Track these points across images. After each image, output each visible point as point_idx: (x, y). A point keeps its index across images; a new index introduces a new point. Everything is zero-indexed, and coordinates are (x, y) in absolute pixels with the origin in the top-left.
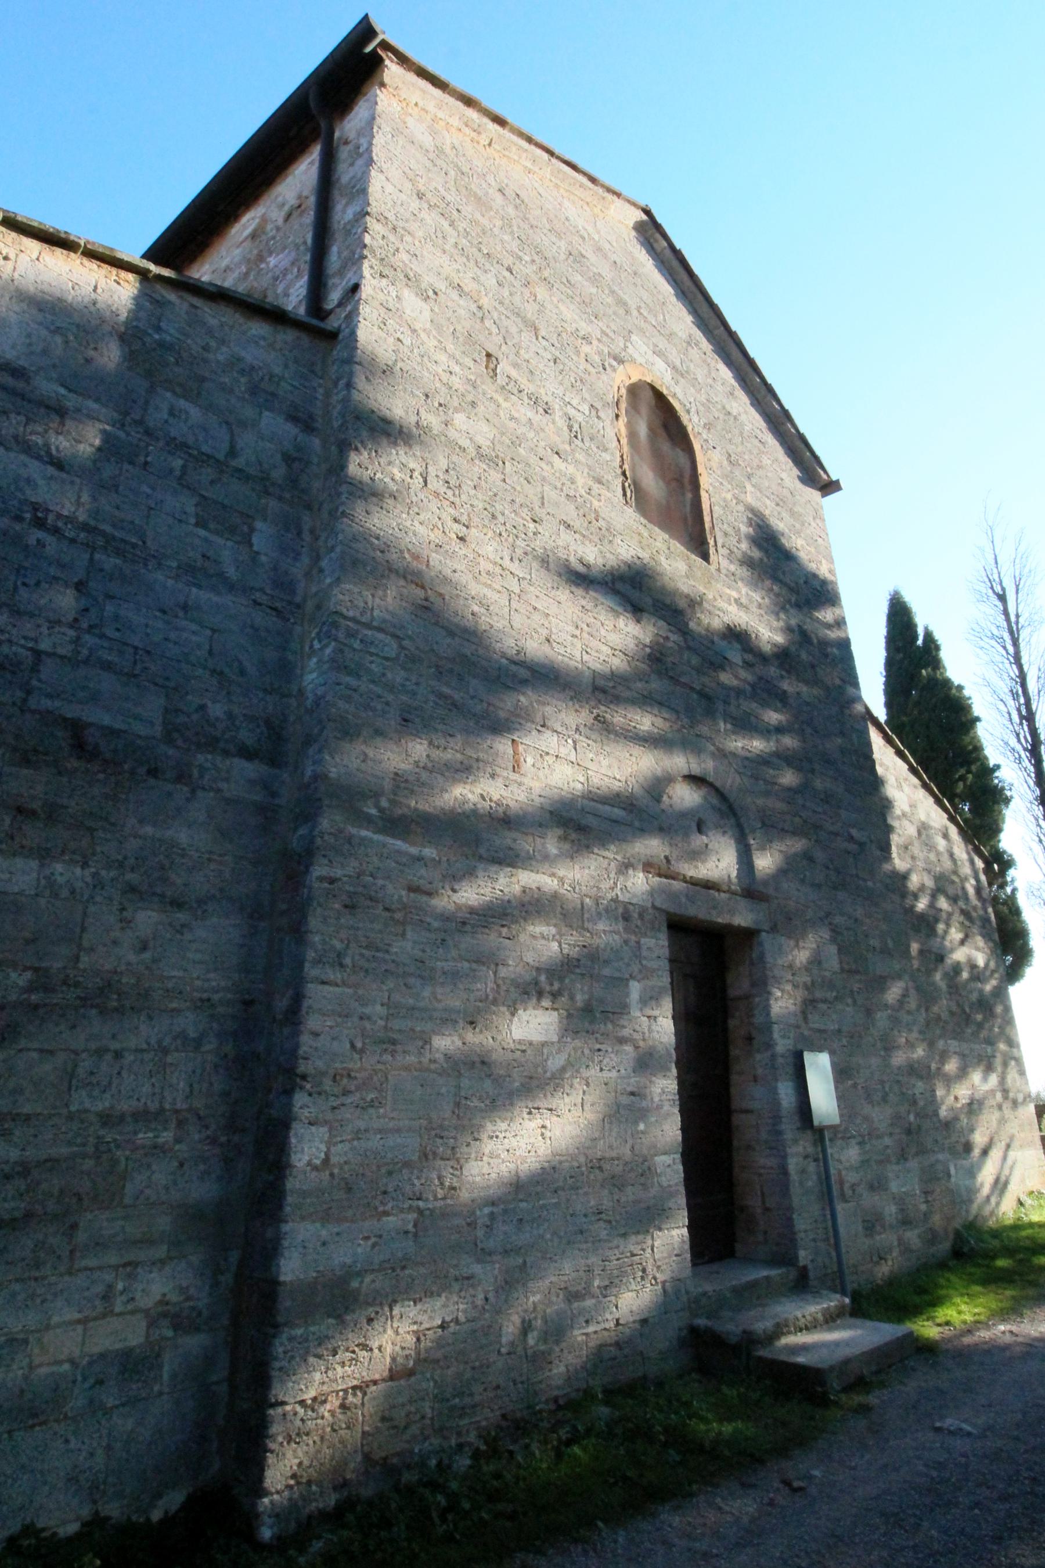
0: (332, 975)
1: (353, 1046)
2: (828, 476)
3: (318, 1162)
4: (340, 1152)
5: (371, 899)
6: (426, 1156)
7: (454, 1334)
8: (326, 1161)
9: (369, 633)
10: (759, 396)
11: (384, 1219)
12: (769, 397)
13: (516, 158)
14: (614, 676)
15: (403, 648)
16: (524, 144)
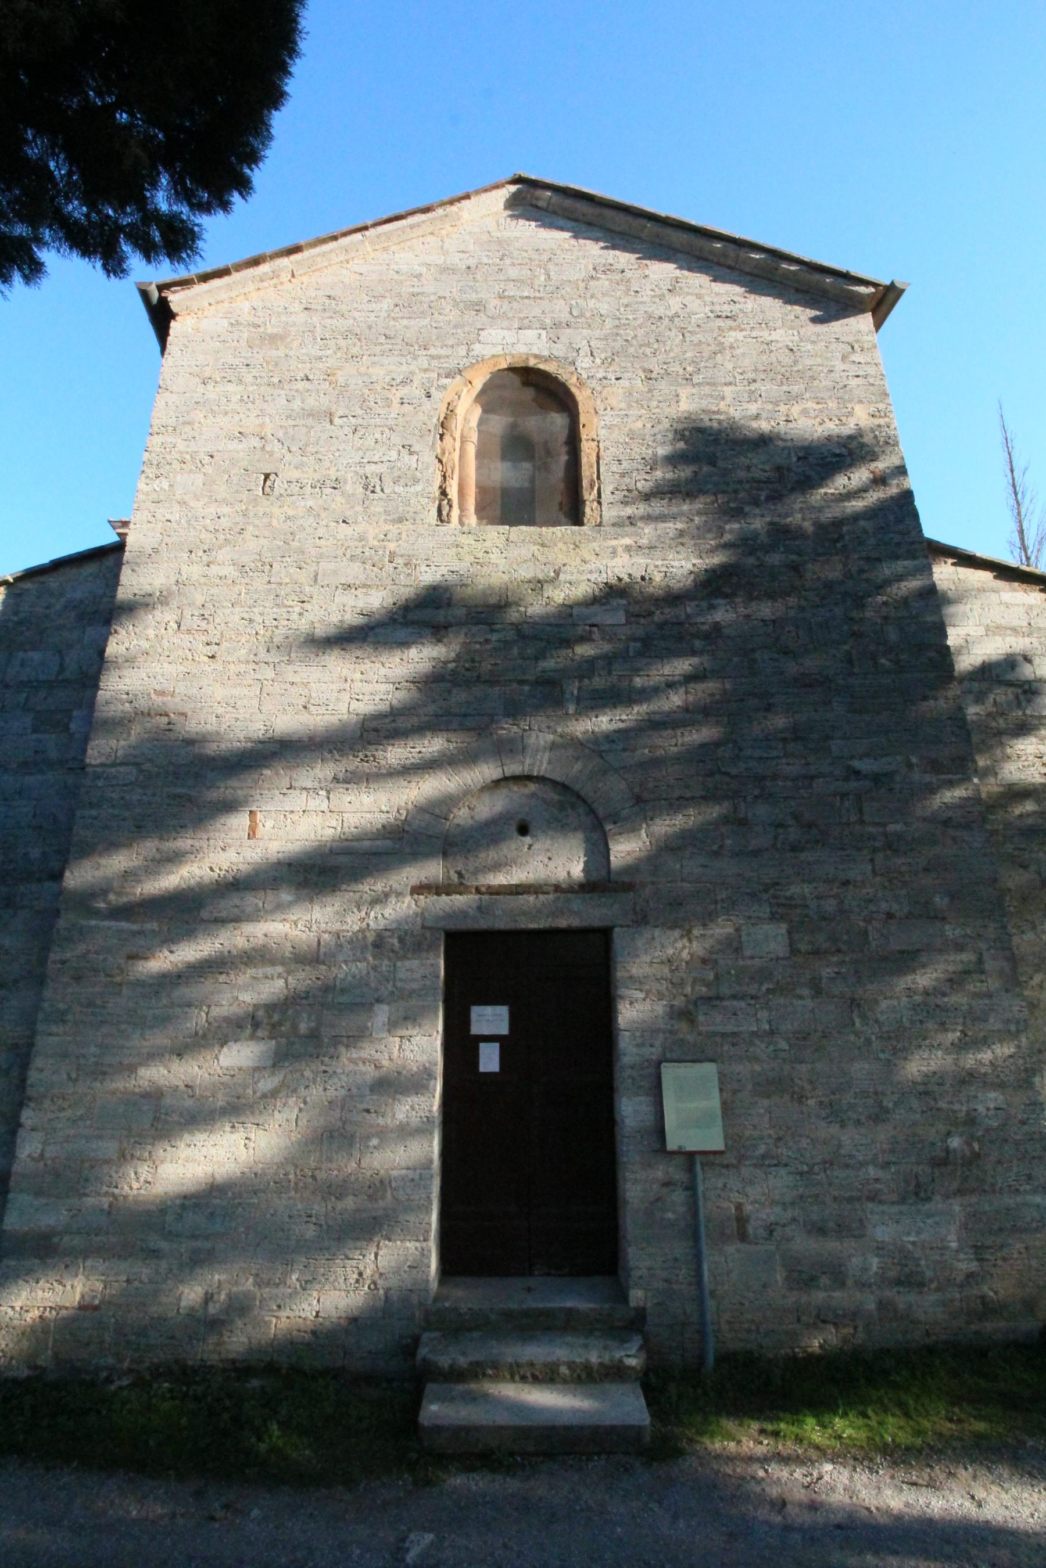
0: (54, 1029)
1: (69, 1078)
2: (875, 285)
3: (36, 1155)
4: (51, 1152)
5: (94, 970)
6: (124, 1156)
7: (137, 1289)
8: (42, 1155)
9: (113, 770)
10: (730, 263)
11: (84, 1199)
12: (743, 253)
13: (326, 264)
14: (394, 713)
15: (142, 771)
16: (333, 245)
